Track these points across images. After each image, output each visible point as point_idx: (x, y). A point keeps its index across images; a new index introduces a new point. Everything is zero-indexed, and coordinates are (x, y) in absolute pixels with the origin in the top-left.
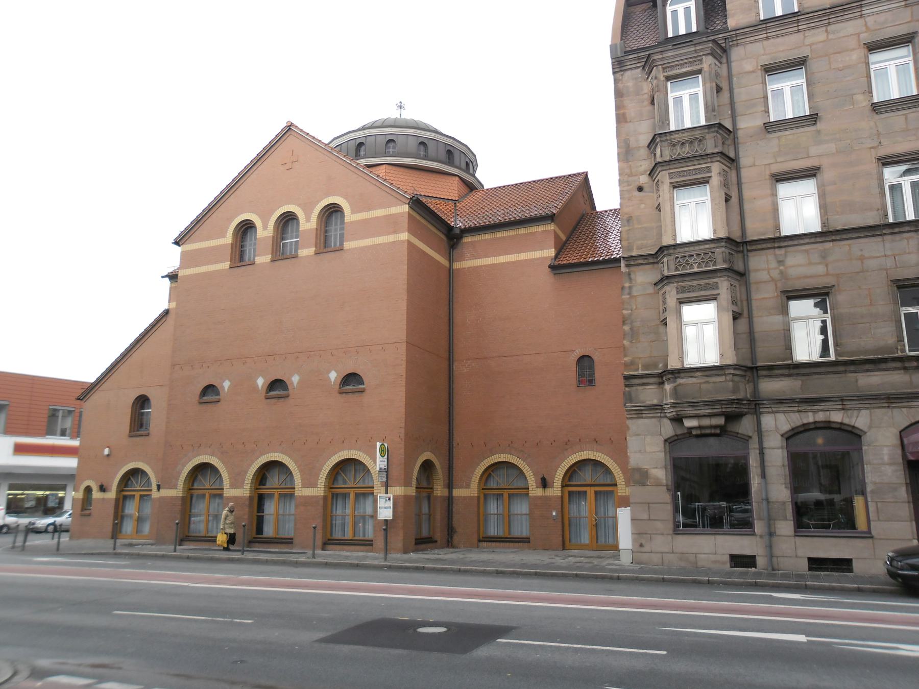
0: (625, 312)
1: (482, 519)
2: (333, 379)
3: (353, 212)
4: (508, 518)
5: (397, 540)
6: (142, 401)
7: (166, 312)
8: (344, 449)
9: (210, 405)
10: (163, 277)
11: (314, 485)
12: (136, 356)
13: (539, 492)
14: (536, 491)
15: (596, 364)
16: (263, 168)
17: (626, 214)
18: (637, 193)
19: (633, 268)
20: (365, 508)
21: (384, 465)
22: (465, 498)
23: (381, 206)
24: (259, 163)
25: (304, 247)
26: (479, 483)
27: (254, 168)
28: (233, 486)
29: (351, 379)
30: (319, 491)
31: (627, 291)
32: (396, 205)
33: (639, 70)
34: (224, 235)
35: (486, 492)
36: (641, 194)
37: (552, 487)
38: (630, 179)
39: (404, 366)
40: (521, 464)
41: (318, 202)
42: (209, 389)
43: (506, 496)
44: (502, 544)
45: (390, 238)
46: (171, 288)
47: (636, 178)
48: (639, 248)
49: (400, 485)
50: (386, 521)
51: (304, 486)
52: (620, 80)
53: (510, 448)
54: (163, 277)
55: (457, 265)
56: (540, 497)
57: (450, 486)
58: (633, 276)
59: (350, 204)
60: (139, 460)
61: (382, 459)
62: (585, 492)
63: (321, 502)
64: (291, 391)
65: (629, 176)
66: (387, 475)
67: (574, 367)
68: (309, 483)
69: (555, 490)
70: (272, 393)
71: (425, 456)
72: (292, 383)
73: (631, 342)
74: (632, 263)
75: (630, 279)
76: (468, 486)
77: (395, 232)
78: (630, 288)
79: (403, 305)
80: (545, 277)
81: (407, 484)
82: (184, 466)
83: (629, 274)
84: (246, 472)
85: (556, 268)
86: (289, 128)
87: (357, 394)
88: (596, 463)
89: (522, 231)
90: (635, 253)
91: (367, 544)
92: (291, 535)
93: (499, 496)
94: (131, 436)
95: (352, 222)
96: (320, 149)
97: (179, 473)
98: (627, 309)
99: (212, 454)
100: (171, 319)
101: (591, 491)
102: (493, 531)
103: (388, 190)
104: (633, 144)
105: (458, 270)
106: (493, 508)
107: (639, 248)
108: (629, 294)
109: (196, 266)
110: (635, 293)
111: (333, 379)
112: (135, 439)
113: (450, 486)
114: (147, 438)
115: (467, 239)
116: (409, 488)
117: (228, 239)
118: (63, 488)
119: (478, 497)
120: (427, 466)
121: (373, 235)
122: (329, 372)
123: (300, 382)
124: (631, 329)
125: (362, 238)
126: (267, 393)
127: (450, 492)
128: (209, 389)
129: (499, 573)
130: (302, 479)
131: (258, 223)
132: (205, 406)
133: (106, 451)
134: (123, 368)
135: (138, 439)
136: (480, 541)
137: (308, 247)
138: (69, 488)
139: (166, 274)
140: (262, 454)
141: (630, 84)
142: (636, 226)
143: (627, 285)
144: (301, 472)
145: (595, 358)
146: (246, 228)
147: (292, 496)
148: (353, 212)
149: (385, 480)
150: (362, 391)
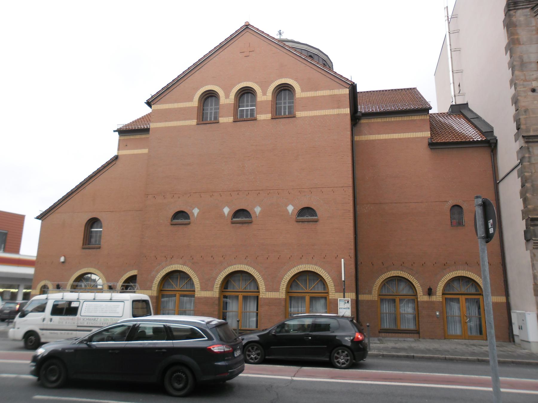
0: (526, 174)
1: (445, 319)
2: (290, 211)
3: (303, 90)
6: (93, 222)
7: (116, 158)
8: (302, 263)
9: (181, 227)
10: (114, 131)
11: (277, 290)
12: (89, 188)
13: (426, 298)
14: (422, 297)
15: (464, 211)
16: (224, 54)
17: (523, 107)
18: (531, 93)
19: (530, 144)
20: (408, 314)
22: (368, 301)
23: (325, 88)
24: (221, 50)
25: (261, 113)
27: (217, 53)
28: (203, 289)
29: (306, 212)
31: (527, 159)
32: (339, 89)
33: (528, 10)
34: (191, 100)
36: (534, 94)
37: (435, 295)
38: (525, 83)
41: (272, 82)
42: (181, 215)
43: (397, 300)
44: (396, 335)
45: (335, 112)
46: (120, 140)
47: (529, 83)
48: (534, 131)
51: (268, 290)
52: (513, 16)
53: (402, 267)
54: (114, 131)
56: (427, 302)
58: (531, 149)
59: (300, 85)
60: (91, 267)
62: (458, 299)
64: (254, 219)
65: (524, 81)
67: (448, 213)
68: (273, 287)
69: (438, 297)
70: (234, 220)
72: (255, 212)
73: (533, 195)
74: (531, 140)
75: (529, 152)
76: (370, 293)
77: (339, 107)
78: (529, 157)
80: (424, 151)
82: (158, 272)
83: (528, 148)
84: (215, 279)
85: (432, 145)
86: (247, 27)
87: (311, 223)
88: (400, 279)
89: (406, 118)
90: (532, 133)
94: (83, 248)
96: (273, 44)
97: (154, 278)
98: (528, 172)
99: (184, 264)
100: (118, 162)
101: (462, 298)
102: (386, 325)
103: (332, 77)
104: (526, 59)
106: (386, 308)
107: (534, 131)
108: (529, 162)
109: (166, 121)
110: (533, 161)
111: (290, 211)
112: (87, 251)
114: (98, 250)
115: (363, 121)
117: (195, 103)
118: (18, 287)
121: (321, 108)
122: (287, 205)
124: (532, 186)
125: (310, 110)
126: (172, 221)
128: (181, 215)
129: (445, 360)
130: (265, 285)
132: (176, 227)
133: (62, 259)
134: (77, 197)
135: (90, 251)
137: (266, 113)
138: (22, 287)
139: (116, 129)
140: (229, 265)
141: (522, 19)
142: (531, 116)
143: (527, 155)
145: (463, 207)
146: (210, 96)
147: (193, 296)
148: (303, 90)
150: (316, 221)
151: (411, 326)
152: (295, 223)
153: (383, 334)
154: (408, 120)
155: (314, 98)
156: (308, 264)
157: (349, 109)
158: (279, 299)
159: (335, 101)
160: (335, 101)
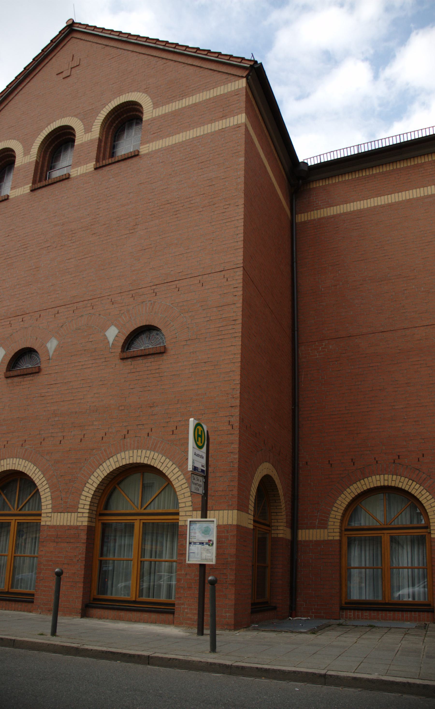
2: (111, 339)
4: (383, 575)
5: (226, 604)
8: (124, 449)
11: (72, 508)
21: (201, 463)
22: (318, 543)
26: (342, 521)
30: (80, 518)
32: (225, 83)
35: (352, 536)
39: (240, 304)
40: (415, 489)
43: (386, 539)
49: (229, 508)
50: (202, 567)
51: (56, 509)
53: (396, 466)
55: (301, 218)
57: (294, 525)
61: (198, 452)
63: (83, 536)
66: (206, 484)
68: (64, 506)
71: (265, 469)
76: (323, 525)
79: (238, 213)
81: (242, 507)
87: (151, 359)
91: (164, 611)
92: (32, 591)
93: (376, 542)
95: (154, 119)
105: (301, 223)
111: (111, 339)
113: (294, 525)
116: (244, 514)
119: (340, 541)
120: (266, 483)
122: (105, 328)
123: (59, 347)
127: (294, 534)
131: (17, 147)
136: (342, 609)
144: (53, 487)
149: (201, 491)
151: (78, 520)
152: (120, 360)
153: (351, 613)
154: (408, 167)
155: (175, 114)
156: (138, 448)
157: (244, 115)
158: (77, 527)
159: (220, 107)
160: (220, 107)
